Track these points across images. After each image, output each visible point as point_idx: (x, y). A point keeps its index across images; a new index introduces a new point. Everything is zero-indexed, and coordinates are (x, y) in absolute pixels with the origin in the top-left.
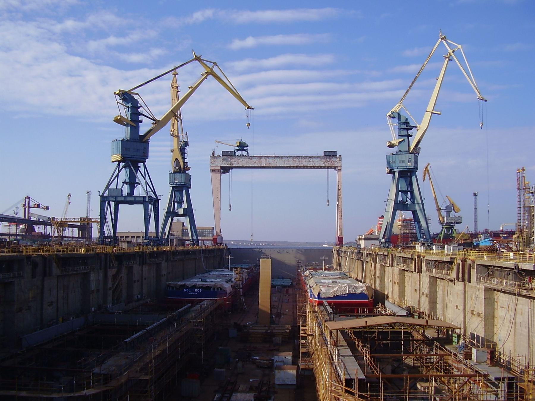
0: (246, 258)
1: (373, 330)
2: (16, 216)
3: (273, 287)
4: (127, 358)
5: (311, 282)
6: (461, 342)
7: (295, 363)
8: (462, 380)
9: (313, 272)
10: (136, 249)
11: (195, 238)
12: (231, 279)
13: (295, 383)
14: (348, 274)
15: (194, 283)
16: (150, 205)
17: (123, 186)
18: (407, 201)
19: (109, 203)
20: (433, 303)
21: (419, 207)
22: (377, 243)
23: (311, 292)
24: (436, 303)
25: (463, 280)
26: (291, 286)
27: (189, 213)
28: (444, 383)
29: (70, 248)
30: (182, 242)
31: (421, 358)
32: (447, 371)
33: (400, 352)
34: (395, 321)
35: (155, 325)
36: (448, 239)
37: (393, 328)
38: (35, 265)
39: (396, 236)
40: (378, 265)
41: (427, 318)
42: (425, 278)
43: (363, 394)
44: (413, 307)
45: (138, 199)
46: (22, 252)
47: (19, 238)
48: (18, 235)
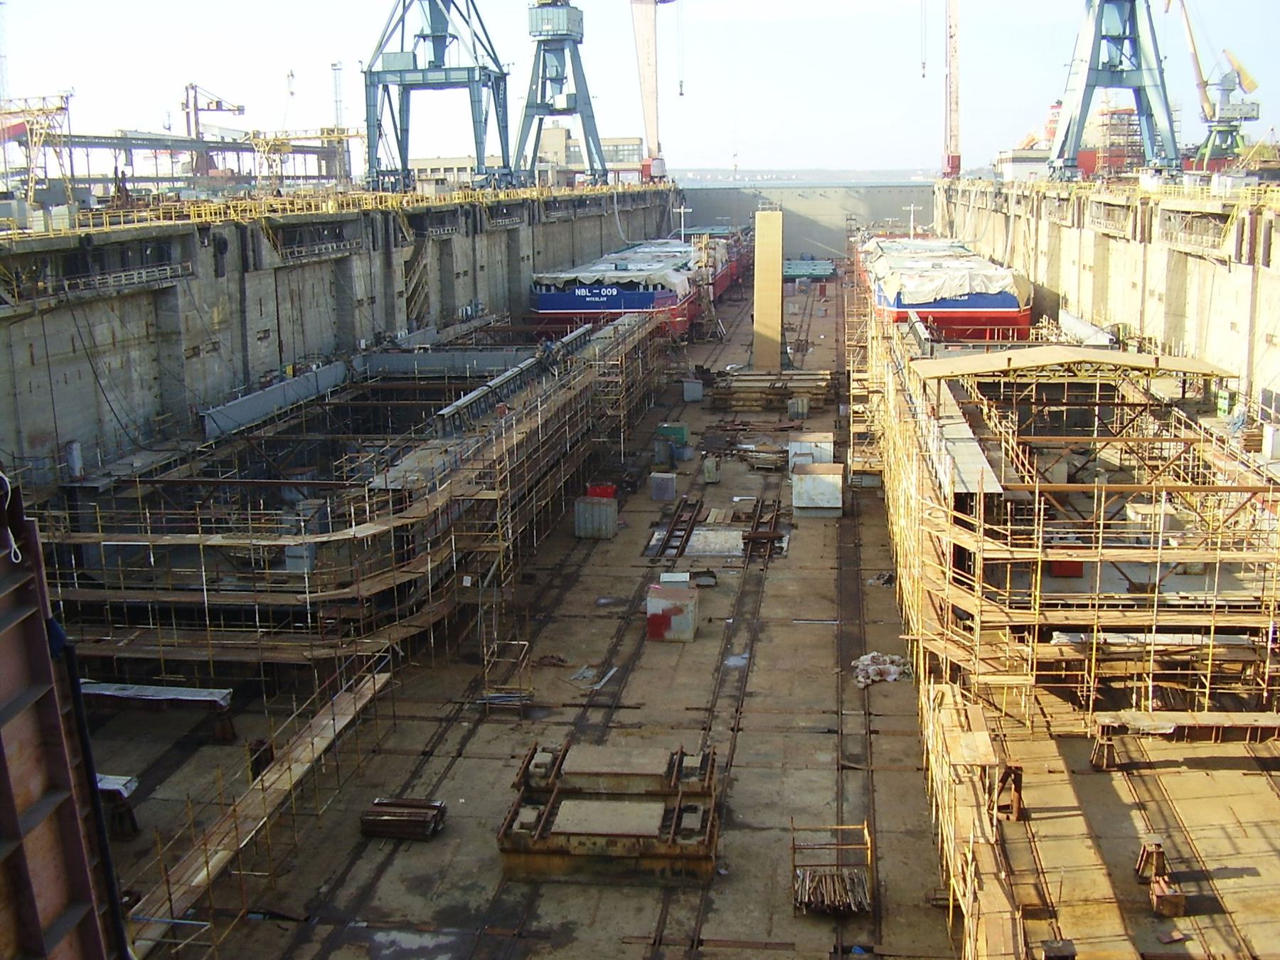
0: (724, 211)
1: (1024, 380)
2: (167, 132)
3: (787, 279)
4: (446, 451)
5: (878, 267)
6: (1239, 409)
7: (838, 458)
8: (1235, 499)
9: (886, 243)
10: (457, 198)
11: (597, 166)
12: (686, 264)
13: (840, 505)
14: (971, 247)
15: (598, 276)
16: (485, 90)
17: (416, 45)
18: (1121, 63)
19: (386, 89)
20: (1176, 315)
21: (1154, 79)
22: (1043, 169)
23: (881, 290)
24: (1183, 315)
25: (1252, 260)
26: (832, 277)
27: (580, 104)
28: (1190, 507)
29: (299, 203)
30: (568, 178)
31: (1140, 446)
32: (1200, 477)
33: (1090, 433)
34: (1080, 359)
35: (508, 374)
36: (1221, 160)
37: (1075, 375)
38: (220, 246)
39: (1092, 153)
40: (1044, 225)
41: (1159, 351)
42: (1159, 250)
43: (995, 528)
44: (1125, 327)
45: (454, 76)
46: (188, 217)
47: (179, 185)
48: (178, 179)
